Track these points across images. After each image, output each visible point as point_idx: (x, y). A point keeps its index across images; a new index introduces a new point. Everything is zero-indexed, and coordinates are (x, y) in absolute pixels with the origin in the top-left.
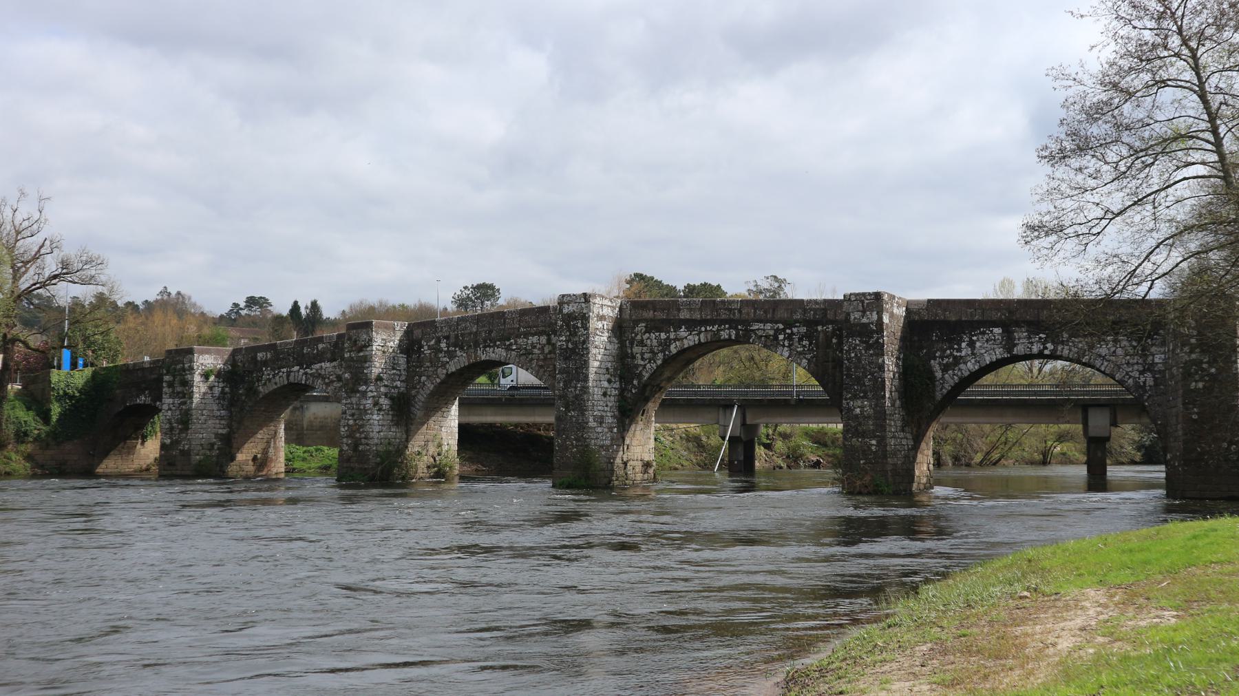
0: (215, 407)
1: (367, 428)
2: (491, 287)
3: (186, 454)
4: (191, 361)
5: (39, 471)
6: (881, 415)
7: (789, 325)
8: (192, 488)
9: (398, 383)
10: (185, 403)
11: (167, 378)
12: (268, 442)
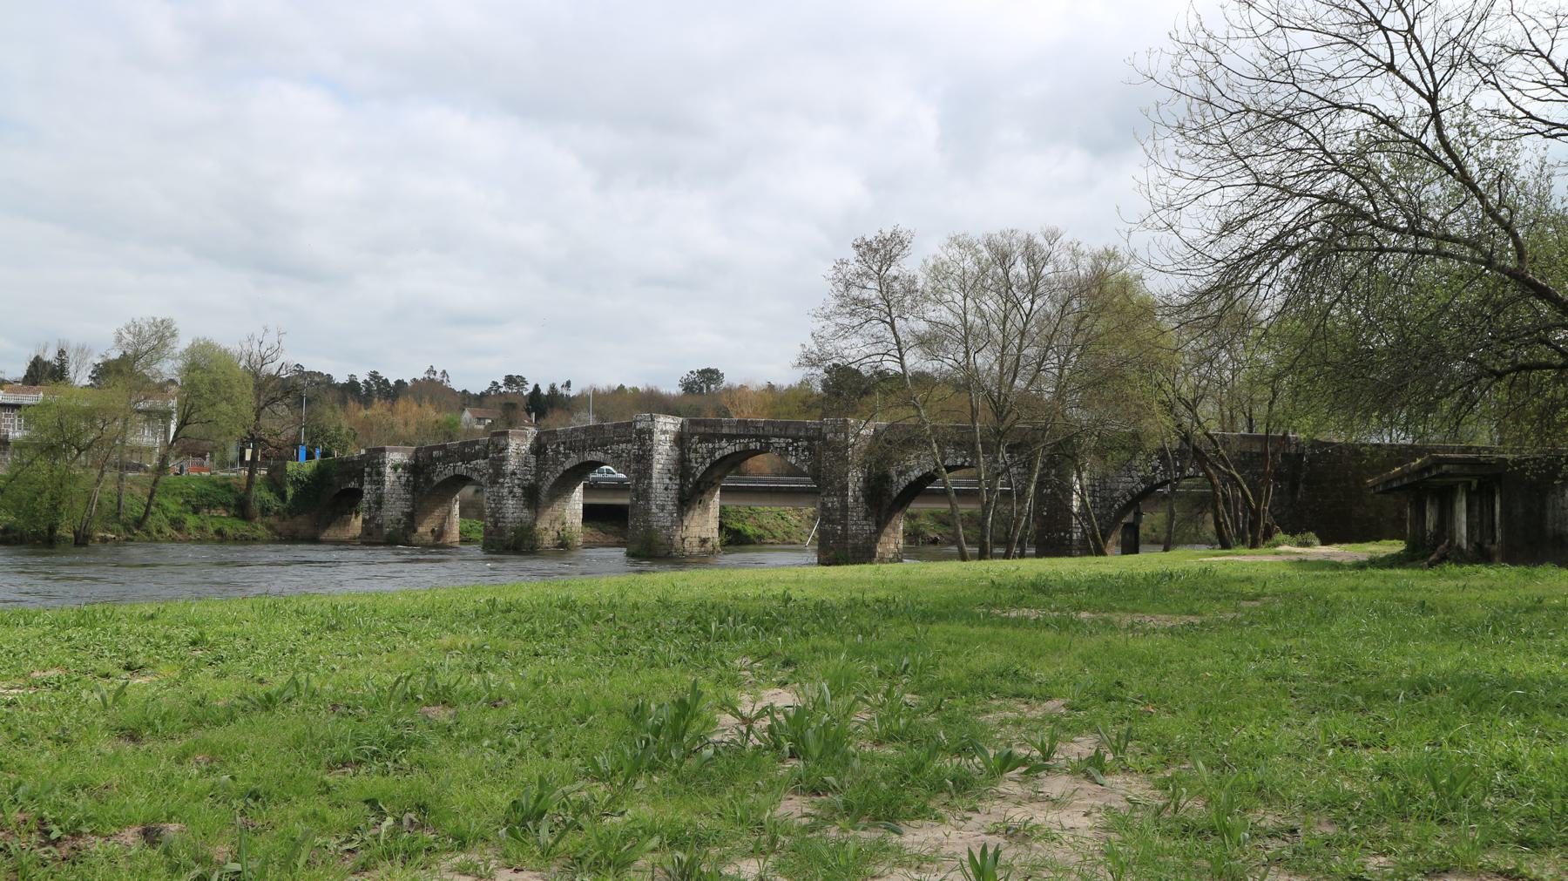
0: (402, 492)
2: (715, 372)
3: (380, 527)
4: (384, 457)
7: (796, 439)
8: (321, 556)
9: (529, 477)
10: (379, 489)
11: (367, 469)
12: (444, 519)
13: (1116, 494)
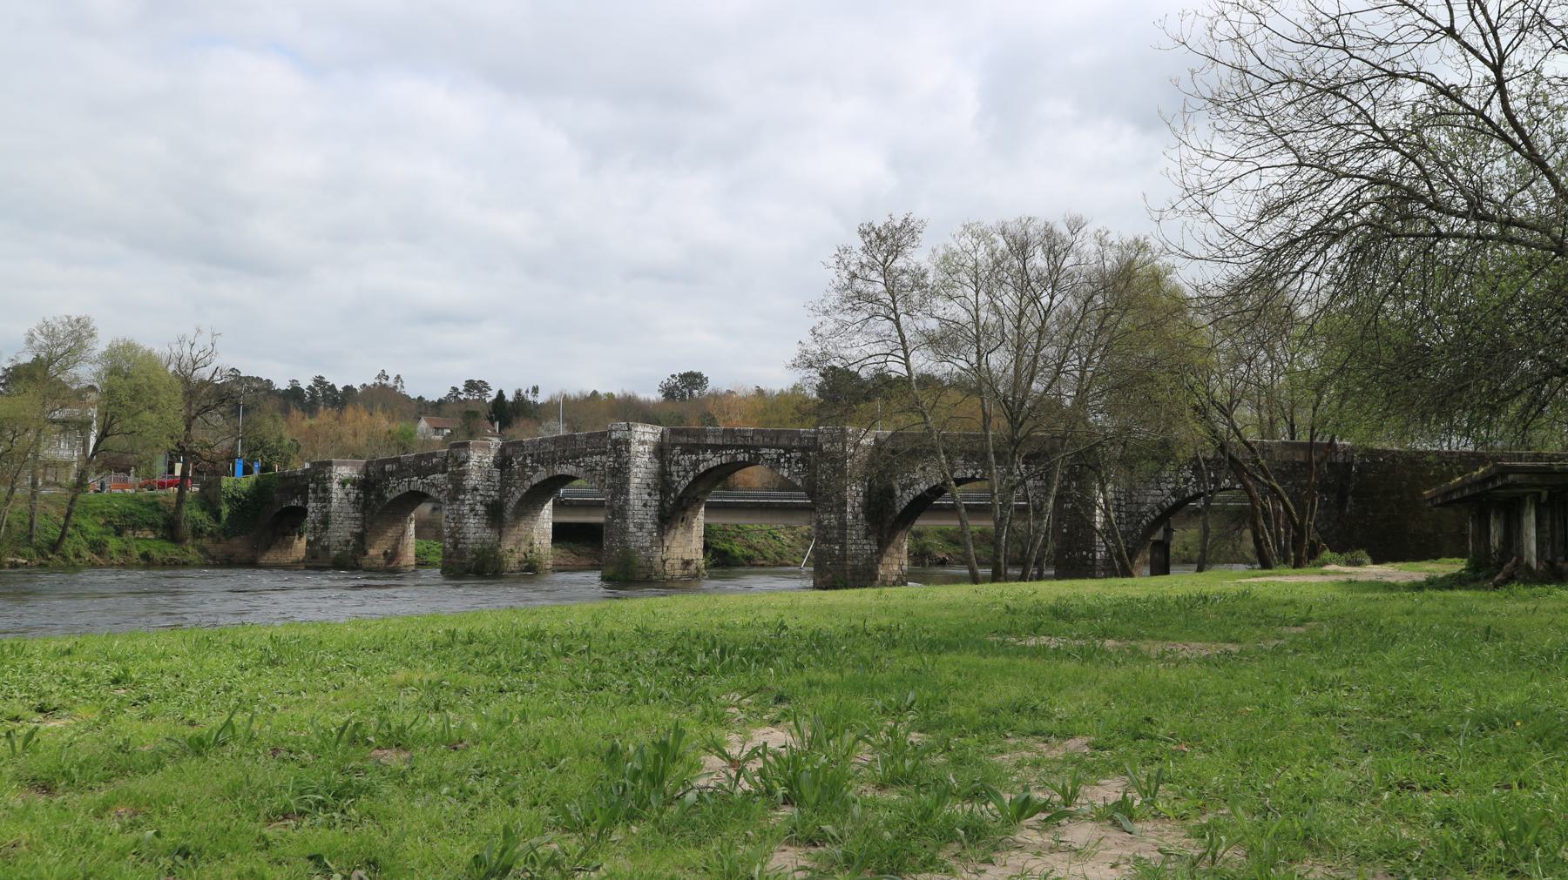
0: (351, 510)
1: (465, 530)
2: (699, 376)
3: (326, 549)
4: (331, 472)
5: (211, 562)
6: (843, 526)
7: (788, 450)
10: (325, 507)
11: (311, 485)
13: (1144, 509)
